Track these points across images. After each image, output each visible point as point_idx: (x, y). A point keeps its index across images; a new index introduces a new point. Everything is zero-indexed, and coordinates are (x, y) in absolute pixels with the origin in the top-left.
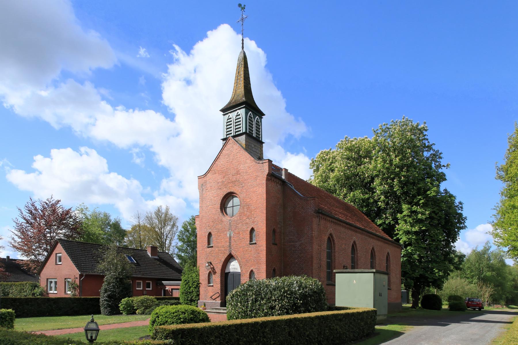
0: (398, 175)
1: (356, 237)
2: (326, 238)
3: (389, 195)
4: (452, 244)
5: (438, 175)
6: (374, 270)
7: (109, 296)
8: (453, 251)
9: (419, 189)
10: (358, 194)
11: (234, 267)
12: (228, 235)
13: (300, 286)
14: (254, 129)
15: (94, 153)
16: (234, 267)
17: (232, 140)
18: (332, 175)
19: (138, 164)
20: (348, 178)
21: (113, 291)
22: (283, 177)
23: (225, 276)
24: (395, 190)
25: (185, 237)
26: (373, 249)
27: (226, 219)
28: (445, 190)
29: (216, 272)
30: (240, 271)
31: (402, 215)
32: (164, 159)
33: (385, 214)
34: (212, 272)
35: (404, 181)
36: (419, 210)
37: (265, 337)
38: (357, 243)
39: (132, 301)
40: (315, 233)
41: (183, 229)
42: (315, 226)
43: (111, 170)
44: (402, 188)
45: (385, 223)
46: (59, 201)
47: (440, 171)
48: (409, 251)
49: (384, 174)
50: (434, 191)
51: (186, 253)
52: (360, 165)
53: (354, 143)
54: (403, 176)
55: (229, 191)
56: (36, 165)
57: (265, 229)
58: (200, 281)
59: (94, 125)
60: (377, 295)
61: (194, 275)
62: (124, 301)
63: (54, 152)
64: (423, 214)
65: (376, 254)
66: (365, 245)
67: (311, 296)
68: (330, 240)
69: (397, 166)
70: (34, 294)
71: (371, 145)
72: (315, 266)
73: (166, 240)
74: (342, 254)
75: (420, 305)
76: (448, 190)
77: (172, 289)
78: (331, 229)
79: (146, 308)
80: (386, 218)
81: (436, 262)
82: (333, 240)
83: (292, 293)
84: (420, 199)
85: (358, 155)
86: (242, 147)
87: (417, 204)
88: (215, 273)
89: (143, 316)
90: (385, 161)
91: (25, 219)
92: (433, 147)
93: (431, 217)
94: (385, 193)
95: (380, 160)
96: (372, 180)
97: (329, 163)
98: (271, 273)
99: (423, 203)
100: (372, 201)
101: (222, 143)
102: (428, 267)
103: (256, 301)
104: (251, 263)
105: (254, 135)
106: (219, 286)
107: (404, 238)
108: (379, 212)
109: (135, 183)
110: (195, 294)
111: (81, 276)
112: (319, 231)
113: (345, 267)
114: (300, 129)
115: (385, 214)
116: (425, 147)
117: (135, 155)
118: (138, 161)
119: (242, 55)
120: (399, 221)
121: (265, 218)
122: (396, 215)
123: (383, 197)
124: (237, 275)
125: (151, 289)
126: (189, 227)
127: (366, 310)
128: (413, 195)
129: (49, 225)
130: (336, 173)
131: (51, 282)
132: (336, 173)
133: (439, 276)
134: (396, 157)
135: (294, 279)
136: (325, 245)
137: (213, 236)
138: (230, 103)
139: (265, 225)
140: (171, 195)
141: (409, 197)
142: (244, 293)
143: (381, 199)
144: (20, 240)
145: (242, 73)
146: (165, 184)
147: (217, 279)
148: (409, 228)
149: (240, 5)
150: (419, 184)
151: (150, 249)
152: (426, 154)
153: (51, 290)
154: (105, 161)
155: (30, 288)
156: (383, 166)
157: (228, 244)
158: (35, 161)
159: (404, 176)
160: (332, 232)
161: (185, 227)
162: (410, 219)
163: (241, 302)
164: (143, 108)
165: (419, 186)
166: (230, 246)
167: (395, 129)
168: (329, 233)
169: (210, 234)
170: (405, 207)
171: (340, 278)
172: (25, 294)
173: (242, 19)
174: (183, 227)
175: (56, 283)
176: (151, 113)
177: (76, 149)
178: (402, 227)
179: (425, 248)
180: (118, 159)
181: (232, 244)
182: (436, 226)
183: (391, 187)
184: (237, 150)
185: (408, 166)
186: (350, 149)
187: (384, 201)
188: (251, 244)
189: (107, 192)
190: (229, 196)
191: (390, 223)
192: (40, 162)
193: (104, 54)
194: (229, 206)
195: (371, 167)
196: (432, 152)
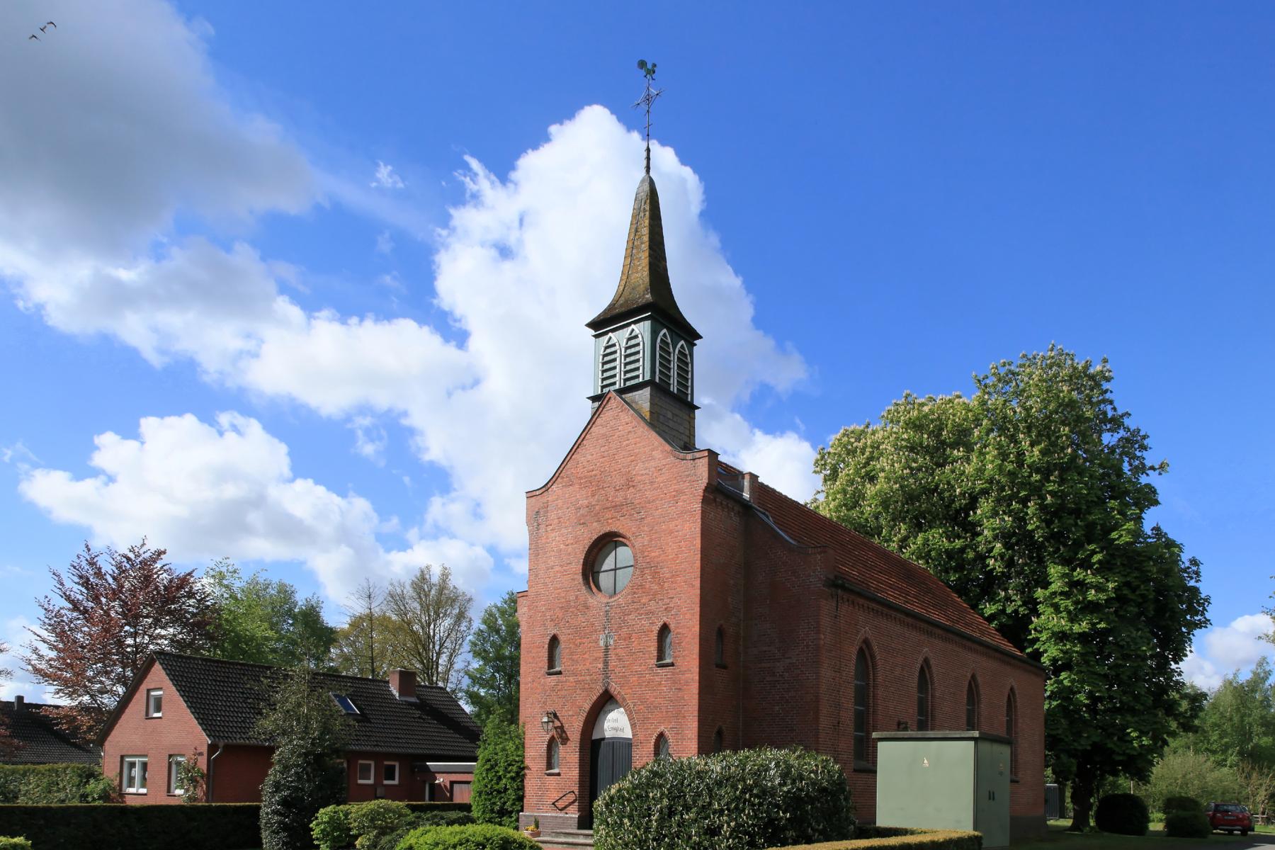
0: (1037, 491)
1: (932, 649)
3: (1014, 540)
4: (1174, 666)
5: (1139, 491)
6: (976, 734)
8: (1177, 682)
9: (1091, 526)
10: (936, 537)
11: (615, 725)
12: (602, 643)
14: (674, 373)
15: (255, 428)
16: (616, 724)
17: (615, 401)
18: (870, 490)
20: (911, 498)
21: (296, 788)
23: (592, 748)
24: (1030, 527)
25: (488, 647)
27: (597, 601)
28: (1157, 529)
29: (568, 739)
30: (628, 734)
31: (1047, 593)
32: (436, 445)
33: (1006, 590)
34: (558, 737)
35: (1051, 505)
36: (1090, 579)
39: (346, 815)
41: (483, 627)
44: (1048, 523)
45: (1003, 611)
47: (1144, 480)
48: (1066, 683)
49: (1002, 489)
50: (1129, 531)
51: (492, 687)
53: (926, 409)
54: (1050, 492)
55: (607, 529)
56: (99, 460)
57: (697, 629)
58: (527, 762)
59: (255, 355)
61: (510, 746)
62: (324, 814)
63: (149, 425)
64: (1100, 588)
67: (812, 800)
69: (1034, 468)
72: (824, 722)
73: (439, 654)
76: (1164, 529)
77: (452, 783)
78: (867, 627)
80: (1008, 599)
81: (1133, 711)
82: (873, 657)
83: (764, 792)
84: (1094, 552)
85: (936, 440)
86: (642, 418)
87: (1086, 564)
88: (565, 740)
90: (1004, 456)
92: (1126, 421)
95: (992, 452)
96: (973, 502)
97: (862, 459)
98: (711, 742)
99: (1099, 562)
100: (971, 555)
101: (589, 407)
103: (671, 813)
105: (674, 388)
106: (575, 773)
107: (1051, 652)
109: (361, 505)
110: (511, 795)
111: (212, 749)
113: (901, 726)
114: (789, 373)
115: (1006, 590)
116: (1105, 420)
117: (360, 433)
118: (368, 449)
119: (646, 187)
120: (1041, 608)
121: (697, 600)
122: (1031, 591)
123: (999, 545)
124: (624, 747)
125: (396, 782)
126: (500, 622)
129: (132, 616)
130: (881, 484)
131: (132, 765)
132: (881, 484)
133: (1142, 746)
134: (1032, 445)
135: (771, 757)
136: (851, 668)
137: (562, 645)
139: (697, 617)
140: (453, 536)
141: (1065, 545)
142: (640, 794)
143: (996, 551)
144: (53, 654)
145: (645, 231)
146: (437, 508)
147: (570, 756)
149: (642, 64)
150: (1090, 513)
151: (397, 677)
152: (1108, 439)
153: (131, 784)
154: (283, 449)
157: (601, 666)
158: (97, 448)
159: (1053, 494)
161: (490, 620)
162: (1069, 603)
163: (631, 817)
164: (386, 315)
165: (1091, 518)
167: (1030, 376)
168: (860, 637)
169: (554, 641)
170: (1054, 571)
171: (892, 755)
172: (62, 795)
173: (648, 99)
174: (484, 622)
175: (145, 766)
177: (207, 417)
178: (1048, 621)
179: (1105, 676)
180: (317, 443)
183: (1021, 520)
187: (1002, 556)
188: (659, 666)
189: (287, 529)
190: (606, 542)
191: (1016, 611)
193: (301, 181)
194: (605, 567)
195: (969, 469)
196: (1122, 433)
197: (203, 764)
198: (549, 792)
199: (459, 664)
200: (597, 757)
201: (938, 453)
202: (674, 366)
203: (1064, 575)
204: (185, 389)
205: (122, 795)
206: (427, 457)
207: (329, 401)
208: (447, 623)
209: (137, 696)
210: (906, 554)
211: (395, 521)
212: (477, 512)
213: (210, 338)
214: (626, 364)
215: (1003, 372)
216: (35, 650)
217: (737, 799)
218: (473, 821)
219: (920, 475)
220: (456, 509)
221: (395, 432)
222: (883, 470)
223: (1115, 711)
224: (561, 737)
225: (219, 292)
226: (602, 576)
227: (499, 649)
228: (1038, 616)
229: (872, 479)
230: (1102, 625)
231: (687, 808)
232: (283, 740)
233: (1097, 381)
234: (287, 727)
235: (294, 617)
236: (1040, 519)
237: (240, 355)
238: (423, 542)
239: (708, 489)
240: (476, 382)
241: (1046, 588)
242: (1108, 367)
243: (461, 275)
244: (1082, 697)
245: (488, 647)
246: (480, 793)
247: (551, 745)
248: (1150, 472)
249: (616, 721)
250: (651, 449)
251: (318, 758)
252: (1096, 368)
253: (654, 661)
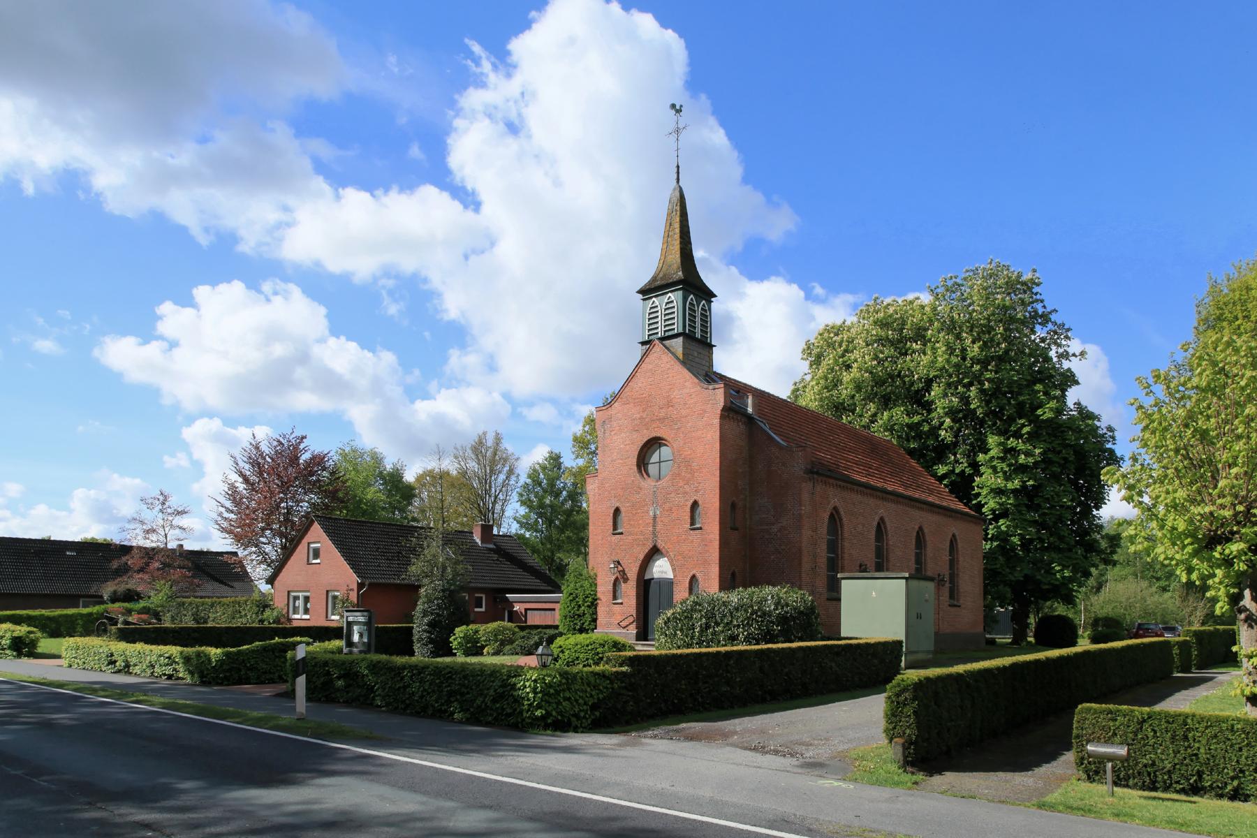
0: (978, 379)
1: (885, 510)
2: (826, 516)
3: (961, 415)
4: (1095, 512)
5: (1062, 374)
6: (907, 575)
7: (430, 624)
8: (1097, 526)
9: (1021, 405)
10: (899, 414)
12: (651, 513)
13: (777, 604)
14: (698, 324)
15: (296, 292)
16: (661, 569)
17: (658, 347)
18: (846, 377)
19: (401, 318)
20: (879, 382)
21: (438, 615)
22: (750, 410)
23: (645, 586)
24: (972, 406)
25: (532, 497)
26: (921, 528)
27: (648, 484)
28: (1078, 404)
30: (671, 576)
31: (987, 457)
32: (454, 304)
33: (955, 454)
34: (622, 577)
35: (989, 389)
36: (1021, 446)
37: (728, 672)
38: (886, 519)
39: (477, 632)
40: (806, 509)
41: (529, 481)
42: (806, 496)
43: (335, 331)
44: (988, 403)
45: (953, 471)
46: (304, 438)
47: (1066, 365)
48: (1003, 528)
49: (950, 376)
50: (1051, 409)
51: (536, 531)
52: (906, 354)
53: (891, 310)
54: (987, 380)
55: (654, 435)
56: (164, 328)
57: (717, 504)
58: (599, 595)
59: (289, 225)
60: (913, 616)
61: (586, 584)
62: (460, 631)
63: (202, 293)
64: (1028, 454)
65: (927, 538)
66: (902, 524)
67: (794, 619)
68: (835, 518)
69: (975, 361)
70: (262, 621)
72: (806, 566)
73: (495, 503)
74: (858, 544)
75: (1031, 639)
76: (1084, 403)
77: (526, 610)
78: (835, 498)
79: (503, 643)
80: (957, 461)
81: (1059, 550)
82: (841, 520)
83: (764, 614)
84: (1023, 426)
85: (898, 335)
86: (678, 359)
87: (1017, 435)
88: (626, 580)
90: (951, 350)
91: (241, 474)
92: (1053, 317)
93: (1046, 461)
94: (951, 413)
95: (941, 348)
96: (929, 382)
97: (840, 351)
98: (728, 583)
99: (1028, 433)
100: (926, 428)
101: (640, 350)
102: (1042, 560)
103: (708, 626)
104: (691, 563)
105: (698, 335)
106: (633, 602)
107: (991, 504)
108: (942, 451)
109: (388, 358)
110: (588, 618)
111: (360, 586)
112: (811, 507)
113: (863, 568)
114: (780, 224)
115: (955, 454)
116: (1035, 316)
117: (384, 293)
118: (393, 310)
119: (678, 194)
120: (983, 469)
121: (718, 484)
122: (975, 455)
123: (948, 420)
124: (668, 585)
125: (483, 609)
126: (542, 476)
127: (882, 640)
128: (1008, 417)
129: (285, 487)
130: (855, 373)
131: (296, 598)
132: (855, 373)
133: (1063, 578)
134: (973, 342)
135: (768, 590)
136: (823, 529)
137: (623, 514)
138: (654, 279)
139: (718, 496)
140: (469, 385)
141: (1001, 420)
142: (687, 615)
143: (945, 425)
144: (232, 516)
145: (677, 226)
146: (456, 359)
147: (629, 591)
148: (1000, 482)
149: (673, 106)
150: (1021, 394)
151: (479, 529)
152: (1041, 332)
153: (296, 611)
154: (323, 311)
155: (256, 609)
156: (948, 361)
158: (160, 318)
159: (989, 380)
160: (838, 504)
161: (533, 475)
162: (1004, 465)
163: (681, 630)
164: (408, 186)
165: (1021, 398)
166: (654, 533)
167: (971, 288)
168: (830, 507)
169: (617, 511)
170: (992, 440)
171: (850, 589)
172: (244, 620)
173: (678, 131)
174: (529, 476)
175: (307, 599)
176: (429, 192)
177: (253, 285)
178: (987, 480)
179: (1036, 522)
180: (350, 304)
182: (1056, 478)
183: (965, 400)
184: (667, 365)
185: (1002, 359)
186: (884, 324)
187: (951, 428)
189: (331, 383)
190: (654, 443)
191: (963, 471)
192: (172, 319)
193: (329, 70)
195: (925, 360)
196: (1050, 326)
197: (354, 597)
199: (509, 512)
200: (649, 594)
201: (900, 346)
202: (698, 320)
203: (1000, 444)
204: (224, 260)
205: (290, 620)
206: (446, 317)
207: (363, 267)
208: (502, 477)
209: (300, 547)
210: (875, 427)
211: (417, 372)
212: (491, 366)
213: (250, 214)
215: (950, 283)
216: (220, 514)
217: (748, 618)
218: (561, 634)
219: (886, 364)
220: (472, 360)
221: (416, 292)
222: (856, 361)
223: (1044, 549)
225: (254, 171)
227: (541, 499)
228: (981, 476)
229: (848, 367)
230: (1031, 483)
231: (717, 624)
232: (426, 581)
233: (1028, 286)
234: (430, 569)
235: (383, 478)
236: (981, 400)
237: (280, 226)
238: (443, 391)
239: (725, 409)
240: (493, 244)
241: (986, 453)
242: (1037, 275)
243: (470, 148)
244: (1015, 540)
245: (532, 497)
246: (566, 617)
248: (1072, 358)
250: (684, 383)
251: (452, 592)
252: (1027, 277)
253: (688, 526)
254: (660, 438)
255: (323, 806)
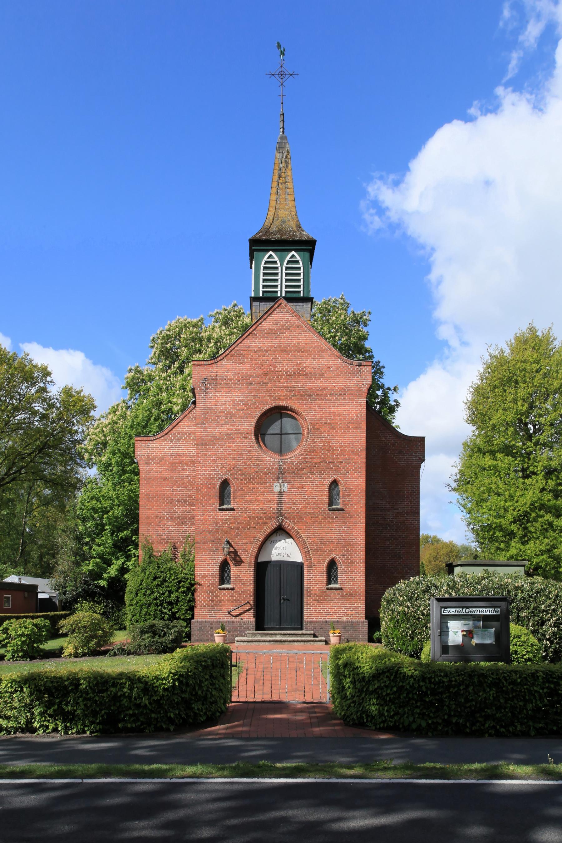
11: (283, 551)
55: (276, 404)
57: (364, 485)
58: (198, 579)
71: (506, 388)
89: (76, 659)
147: (243, 578)
169: (225, 484)
181: (285, 507)
194: (270, 431)
198: (557, 667)
214: (277, 286)
224: (234, 559)
226: (267, 438)
247: (224, 566)
249: (284, 548)
253: (326, 506)
254: (286, 408)
255: (463, 622)
